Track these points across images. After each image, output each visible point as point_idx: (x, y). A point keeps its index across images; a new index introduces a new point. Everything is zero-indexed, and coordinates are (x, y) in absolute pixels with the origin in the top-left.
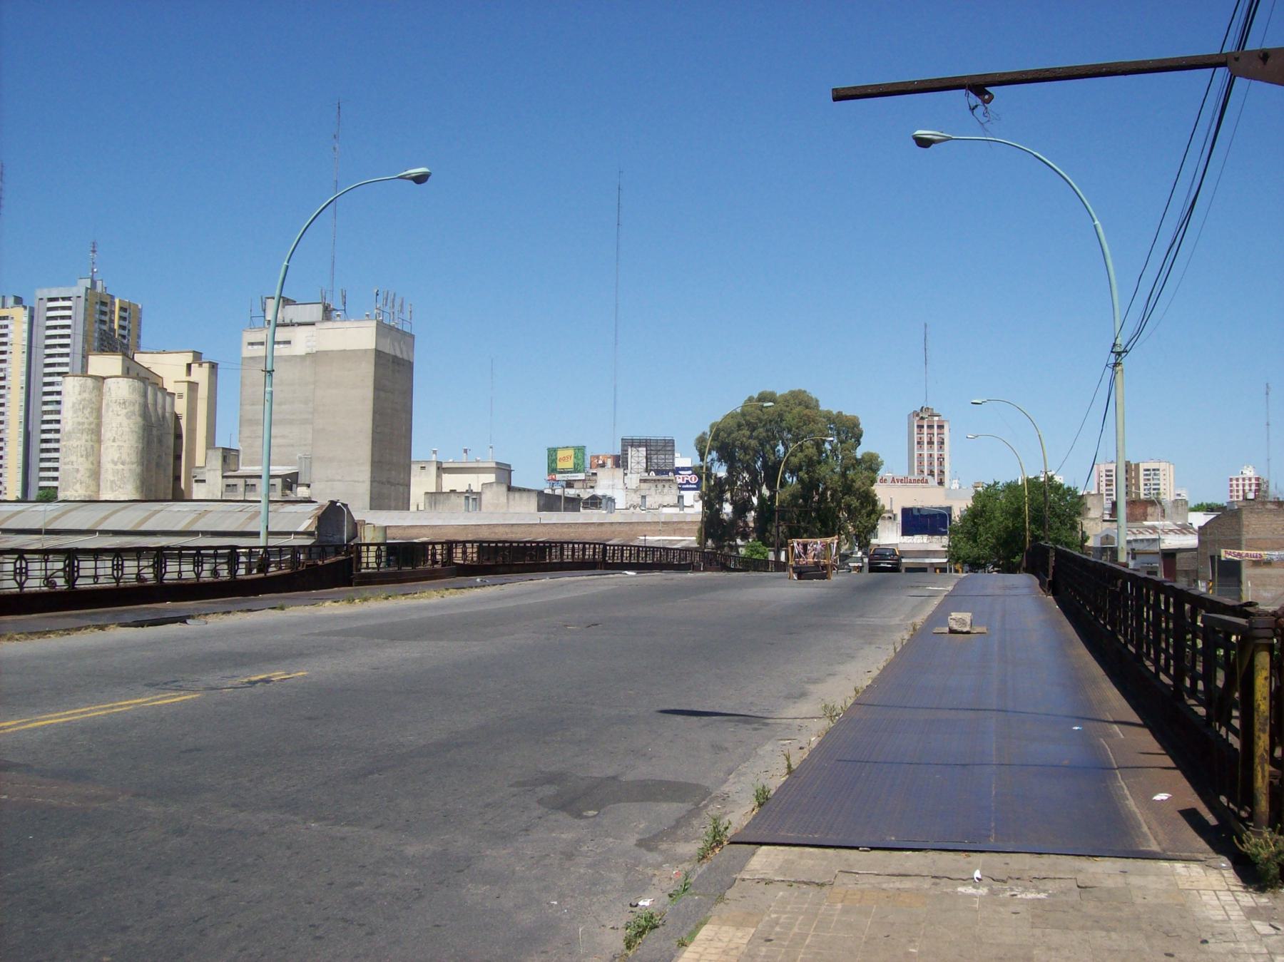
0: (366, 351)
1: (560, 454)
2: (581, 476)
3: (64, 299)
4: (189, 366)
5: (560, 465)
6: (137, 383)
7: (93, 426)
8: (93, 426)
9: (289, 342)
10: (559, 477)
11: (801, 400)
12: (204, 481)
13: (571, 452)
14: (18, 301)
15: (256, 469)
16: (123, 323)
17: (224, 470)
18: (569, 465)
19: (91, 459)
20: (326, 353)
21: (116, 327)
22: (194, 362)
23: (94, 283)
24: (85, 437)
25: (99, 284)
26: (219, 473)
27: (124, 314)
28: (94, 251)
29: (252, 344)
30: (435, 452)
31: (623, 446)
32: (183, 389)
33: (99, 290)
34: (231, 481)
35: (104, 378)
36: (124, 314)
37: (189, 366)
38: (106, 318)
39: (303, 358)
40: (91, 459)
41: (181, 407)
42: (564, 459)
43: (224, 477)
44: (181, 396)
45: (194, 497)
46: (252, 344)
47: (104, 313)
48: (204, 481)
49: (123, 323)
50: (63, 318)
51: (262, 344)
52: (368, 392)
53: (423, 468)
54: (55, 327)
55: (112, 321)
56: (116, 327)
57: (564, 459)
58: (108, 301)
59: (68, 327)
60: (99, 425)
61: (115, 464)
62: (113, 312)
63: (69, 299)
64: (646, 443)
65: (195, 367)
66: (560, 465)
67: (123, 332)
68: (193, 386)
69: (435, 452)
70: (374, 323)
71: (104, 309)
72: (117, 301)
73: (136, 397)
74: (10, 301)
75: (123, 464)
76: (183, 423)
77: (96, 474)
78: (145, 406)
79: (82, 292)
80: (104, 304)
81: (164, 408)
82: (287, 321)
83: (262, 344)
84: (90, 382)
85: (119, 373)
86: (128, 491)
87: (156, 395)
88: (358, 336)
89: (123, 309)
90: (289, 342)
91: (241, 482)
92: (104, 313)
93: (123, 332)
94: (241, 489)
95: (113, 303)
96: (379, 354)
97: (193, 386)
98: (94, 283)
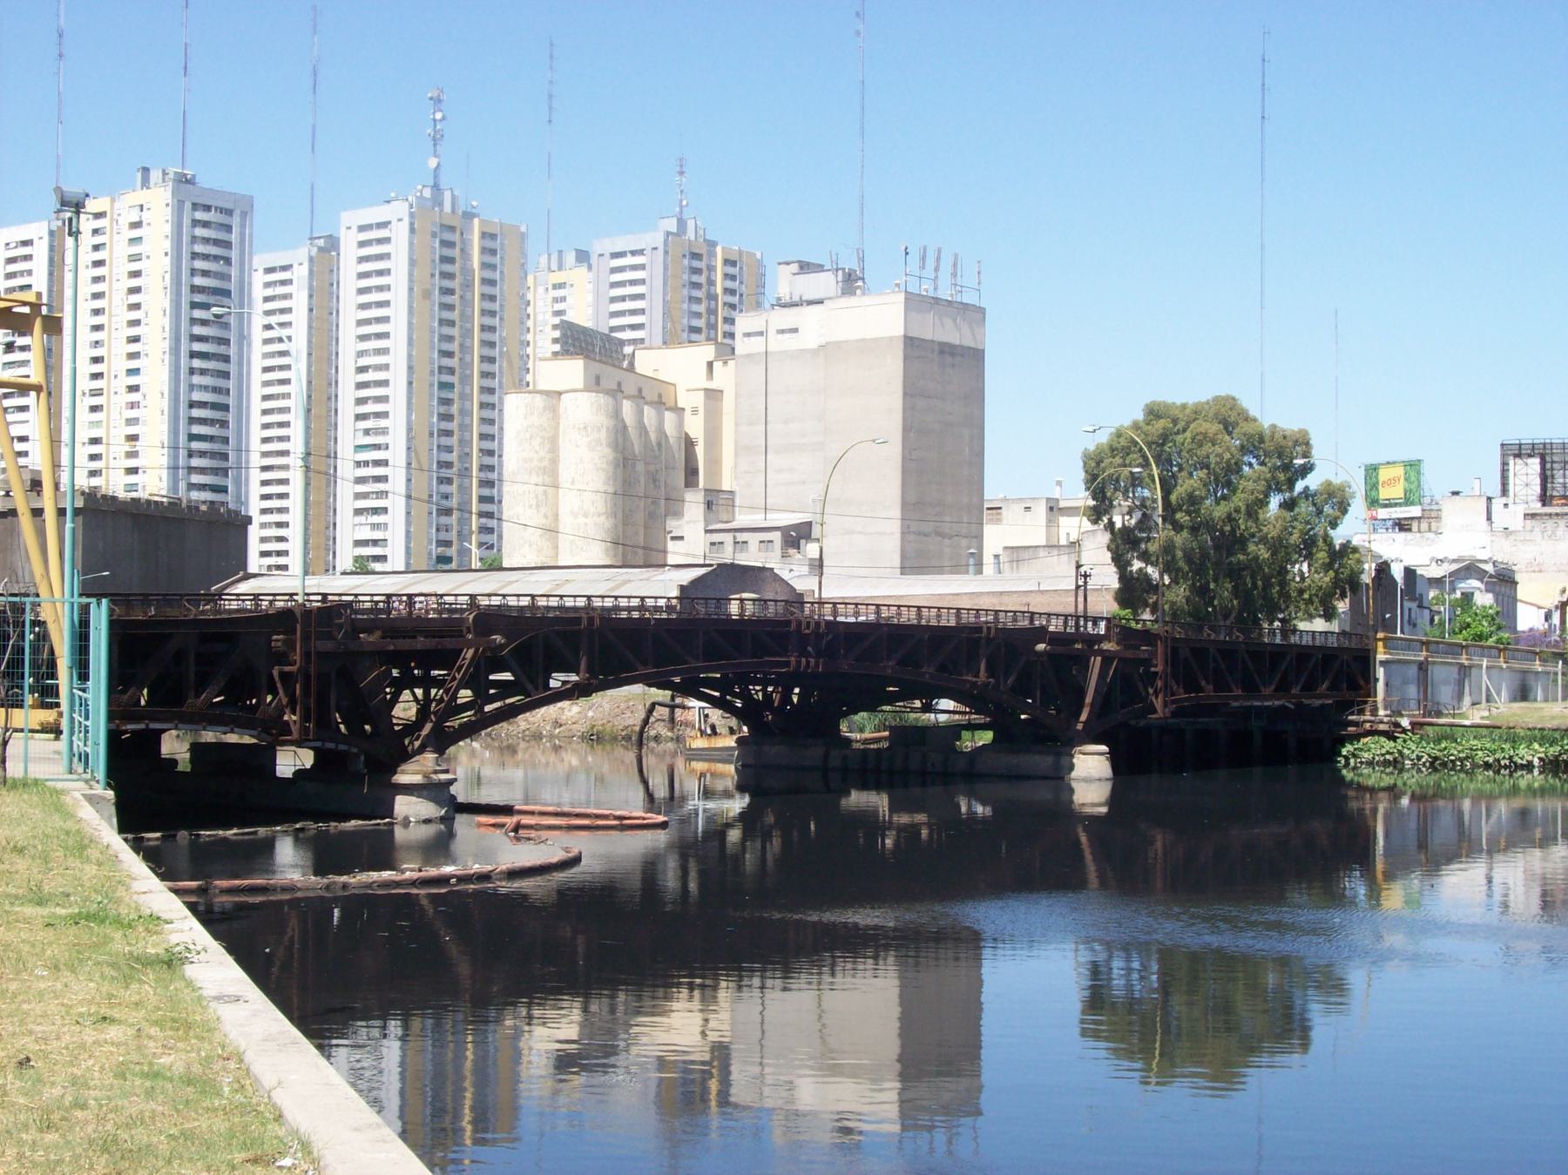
0: (891, 338)
1: (1384, 474)
2: (1415, 511)
3: (633, 253)
4: (710, 365)
5: (1384, 493)
6: (602, 399)
7: (546, 463)
8: (546, 463)
9: (795, 330)
10: (1383, 513)
11: (1228, 416)
12: (681, 538)
13: (1399, 471)
14: (583, 257)
15: (756, 519)
16: (729, 284)
17: (707, 522)
18: (1397, 492)
19: (543, 510)
20: (838, 344)
21: (719, 290)
22: (718, 356)
23: (682, 224)
24: (534, 479)
25: (691, 224)
26: (701, 526)
27: (731, 270)
28: (681, 173)
29: (782, 332)
30: (1059, 483)
31: (1504, 455)
32: (699, 400)
33: (691, 234)
34: (716, 537)
35: (560, 394)
36: (731, 270)
37: (710, 365)
38: (702, 279)
39: (815, 352)
40: (543, 510)
41: (695, 427)
42: (1389, 483)
43: (707, 531)
44: (695, 411)
45: (505, 565)
46: (782, 332)
47: (697, 271)
48: (681, 538)
49: (729, 284)
50: (633, 282)
51: (761, 334)
52: (895, 401)
53: (1028, 509)
54: (623, 299)
55: (711, 283)
56: (719, 290)
57: (1389, 483)
58: (703, 251)
59: (641, 297)
60: (555, 461)
61: (575, 515)
62: (711, 269)
63: (640, 252)
64: (1543, 453)
65: (717, 365)
66: (1384, 493)
67: (730, 299)
68: (713, 395)
69: (1059, 483)
70: (902, 297)
71: (696, 264)
72: (719, 249)
73: (604, 421)
74: (570, 258)
75: (586, 516)
76: (700, 450)
77: (552, 531)
78: (620, 430)
79: (658, 239)
80: (696, 256)
81: (643, 430)
82: (796, 299)
83: (761, 334)
84: (539, 400)
85: (581, 385)
86: (597, 553)
87: (640, 413)
88: (880, 317)
89: (726, 262)
90: (795, 330)
91: (727, 538)
92: (697, 271)
93: (730, 299)
94: (729, 548)
95: (712, 255)
96: (910, 342)
97: (713, 395)
98: (682, 224)
